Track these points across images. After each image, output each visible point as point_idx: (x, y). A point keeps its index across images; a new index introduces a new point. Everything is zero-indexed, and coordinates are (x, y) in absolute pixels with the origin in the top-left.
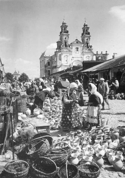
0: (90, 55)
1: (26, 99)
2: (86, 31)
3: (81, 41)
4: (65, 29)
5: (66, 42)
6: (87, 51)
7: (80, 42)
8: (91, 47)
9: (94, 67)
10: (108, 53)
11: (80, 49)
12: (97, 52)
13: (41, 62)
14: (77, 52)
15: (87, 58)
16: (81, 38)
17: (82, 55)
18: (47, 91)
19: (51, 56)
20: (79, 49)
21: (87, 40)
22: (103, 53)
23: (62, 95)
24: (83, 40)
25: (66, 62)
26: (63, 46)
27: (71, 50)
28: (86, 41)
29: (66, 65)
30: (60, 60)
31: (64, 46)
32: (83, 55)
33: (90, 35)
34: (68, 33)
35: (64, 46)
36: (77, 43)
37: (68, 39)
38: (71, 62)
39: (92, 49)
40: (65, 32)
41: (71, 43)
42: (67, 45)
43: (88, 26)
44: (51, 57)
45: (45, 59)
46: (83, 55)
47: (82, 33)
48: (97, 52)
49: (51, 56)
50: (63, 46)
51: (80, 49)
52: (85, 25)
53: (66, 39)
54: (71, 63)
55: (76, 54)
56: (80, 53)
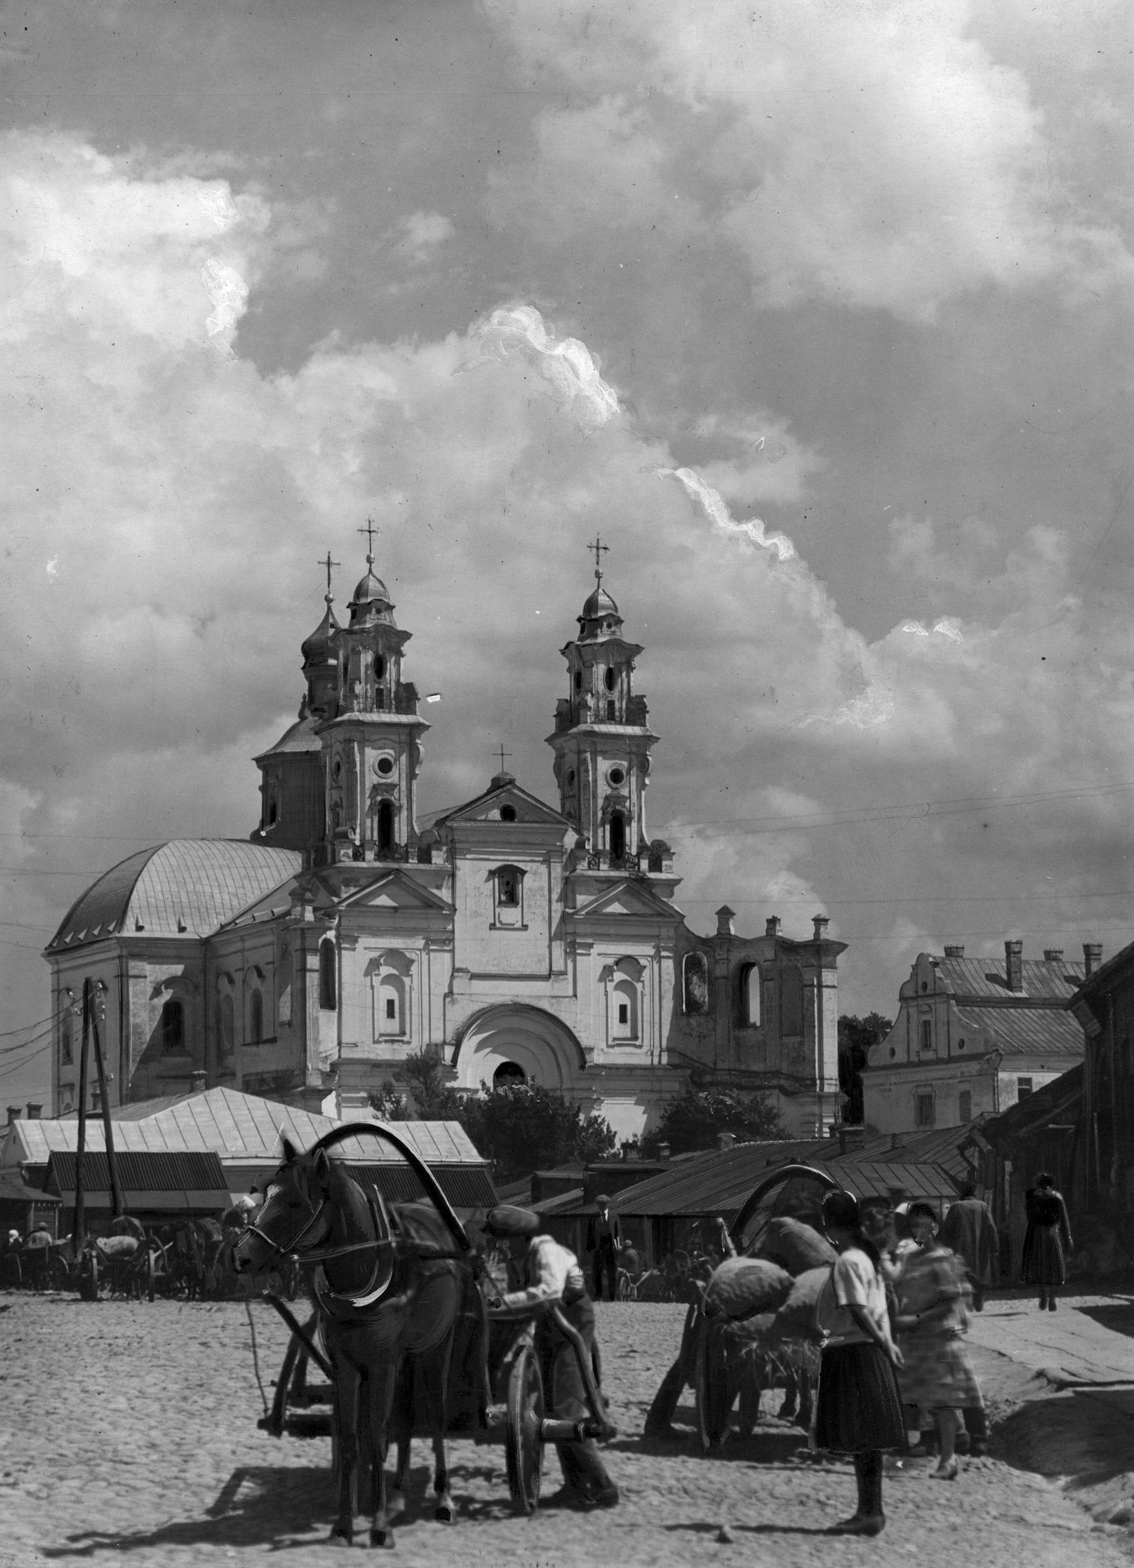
0: (642, 950)
1: (160, 1340)
2: (600, 686)
3: (551, 796)
4: (379, 667)
5: (386, 813)
6: (616, 908)
8: (658, 853)
9: (100, 1205)
11: (539, 880)
12: (725, 914)
14: (510, 915)
15: (385, 970)
16: (550, 755)
17: (558, 949)
18: (512, 1222)
19: (201, 929)
20: (528, 882)
21: (616, 776)
22: (782, 931)
23: (74, 1539)
24: (571, 779)
25: (393, 1026)
26: (358, 855)
27: (445, 894)
30: (329, 1000)
31: (370, 855)
32: (571, 951)
33: (653, 723)
34: (410, 710)
35: (370, 855)
36: (508, 814)
37: (412, 776)
38: (437, 1023)
39: (672, 884)
40: (380, 701)
42: (401, 836)
43: (627, 634)
44: (205, 942)
45: (136, 966)
46: (571, 951)
48: (725, 914)
49: (206, 932)
51: (539, 880)
52: (590, 619)
53: (393, 777)
54: (437, 1037)
55: (495, 933)
56: (539, 930)
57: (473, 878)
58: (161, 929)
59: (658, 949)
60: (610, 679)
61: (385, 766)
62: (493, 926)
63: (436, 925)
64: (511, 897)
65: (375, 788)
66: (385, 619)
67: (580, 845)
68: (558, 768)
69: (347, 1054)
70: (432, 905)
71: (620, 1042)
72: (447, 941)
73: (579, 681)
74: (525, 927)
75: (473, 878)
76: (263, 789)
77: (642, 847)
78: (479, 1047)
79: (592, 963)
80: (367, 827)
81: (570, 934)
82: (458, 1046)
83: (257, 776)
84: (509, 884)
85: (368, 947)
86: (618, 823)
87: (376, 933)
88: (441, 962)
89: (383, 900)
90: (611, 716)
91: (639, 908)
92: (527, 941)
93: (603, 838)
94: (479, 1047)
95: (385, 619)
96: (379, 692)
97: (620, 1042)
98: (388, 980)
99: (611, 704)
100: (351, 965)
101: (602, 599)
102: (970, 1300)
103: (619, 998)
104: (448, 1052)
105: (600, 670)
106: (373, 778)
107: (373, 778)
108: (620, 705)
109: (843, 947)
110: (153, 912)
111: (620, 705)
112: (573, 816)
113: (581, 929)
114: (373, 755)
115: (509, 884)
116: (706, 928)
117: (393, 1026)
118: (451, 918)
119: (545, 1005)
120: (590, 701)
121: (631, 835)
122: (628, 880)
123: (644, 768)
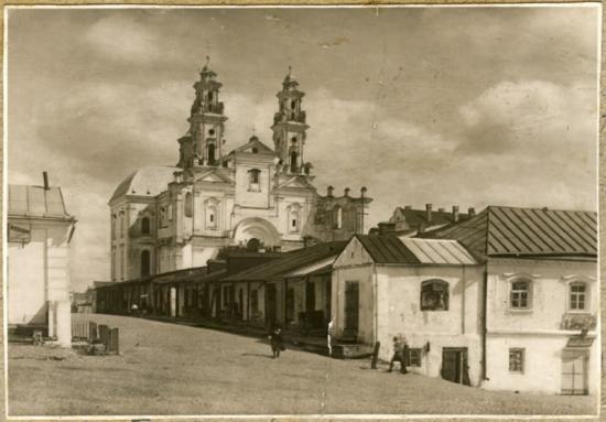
0: (301, 200)
2: (290, 108)
3: (271, 145)
4: (210, 96)
5: (212, 149)
6: (293, 185)
7: (266, 148)
10: (368, 195)
12: (330, 188)
13: (114, 216)
14: (255, 186)
16: (272, 132)
22: (350, 194)
24: (278, 140)
26: (201, 163)
27: (231, 178)
28: (290, 144)
29: (209, 233)
31: (205, 163)
32: (277, 199)
35: (205, 163)
36: (255, 151)
40: (210, 108)
41: (233, 153)
42: (217, 157)
45: (132, 205)
46: (277, 199)
47: (277, 110)
48: (330, 188)
50: (201, 163)
53: (214, 136)
54: (228, 229)
56: (265, 190)
57: (242, 176)
58: (141, 193)
59: (307, 201)
60: (293, 105)
61: (212, 132)
62: (249, 190)
63: (228, 189)
64: (256, 181)
65: (208, 140)
66: (213, 79)
67: (280, 162)
68: (274, 138)
69: (196, 233)
70: (226, 181)
71: (292, 233)
72: (232, 195)
73: (282, 106)
74: (260, 191)
75: (242, 176)
76: (181, 150)
77: (303, 165)
78: (244, 231)
79: (283, 205)
80: (205, 152)
81: (276, 193)
82: (235, 231)
83: (179, 146)
84: (255, 173)
85: (205, 195)
86: (294, 156)
87: (207, 190)
88: (230, 204)
89: (209, 179)
90: (293, 118)
91: (301, 186)
92: (261, 196)
93: (288, 161)
94: (244, 231)
95: (213, 79)
96: (210, 106)
97: (292, 233)
98: (211, 207)
99: (293, 114)
100: (198, 201)
101: (292, 77)
102: (569, 386)
103: (293, 217)
104: (231, 233)
105: (290, 101)
106: (207, 136)
107: (207, 136)
108: (297, 115)
109: (371, 200)
110: (139, 187)
111: (297, 115)
112: (278, 154)
113: (281, 192)
114: (208, 127)
115: (255, 173)
116: (323, 193)
117: (212, 224)
118: (234, 186)
119: (266, 218)
120: (285, 112)
121: (299, 160)
122: (297, 170)
123: (304, 137)
